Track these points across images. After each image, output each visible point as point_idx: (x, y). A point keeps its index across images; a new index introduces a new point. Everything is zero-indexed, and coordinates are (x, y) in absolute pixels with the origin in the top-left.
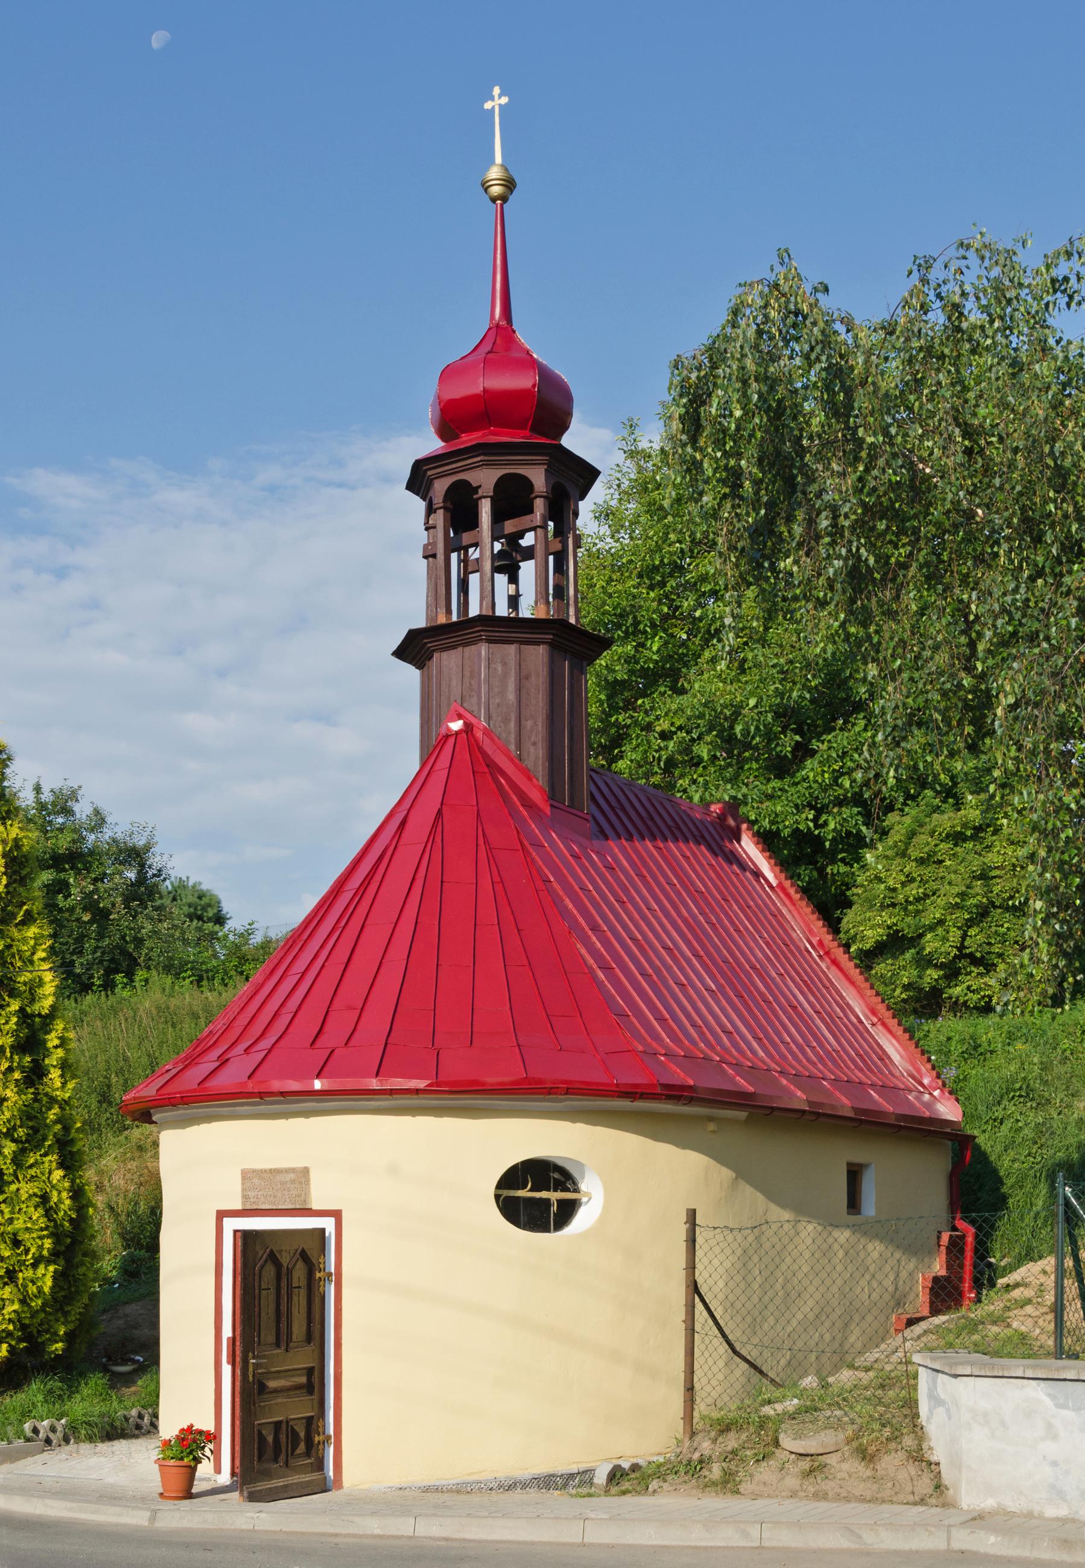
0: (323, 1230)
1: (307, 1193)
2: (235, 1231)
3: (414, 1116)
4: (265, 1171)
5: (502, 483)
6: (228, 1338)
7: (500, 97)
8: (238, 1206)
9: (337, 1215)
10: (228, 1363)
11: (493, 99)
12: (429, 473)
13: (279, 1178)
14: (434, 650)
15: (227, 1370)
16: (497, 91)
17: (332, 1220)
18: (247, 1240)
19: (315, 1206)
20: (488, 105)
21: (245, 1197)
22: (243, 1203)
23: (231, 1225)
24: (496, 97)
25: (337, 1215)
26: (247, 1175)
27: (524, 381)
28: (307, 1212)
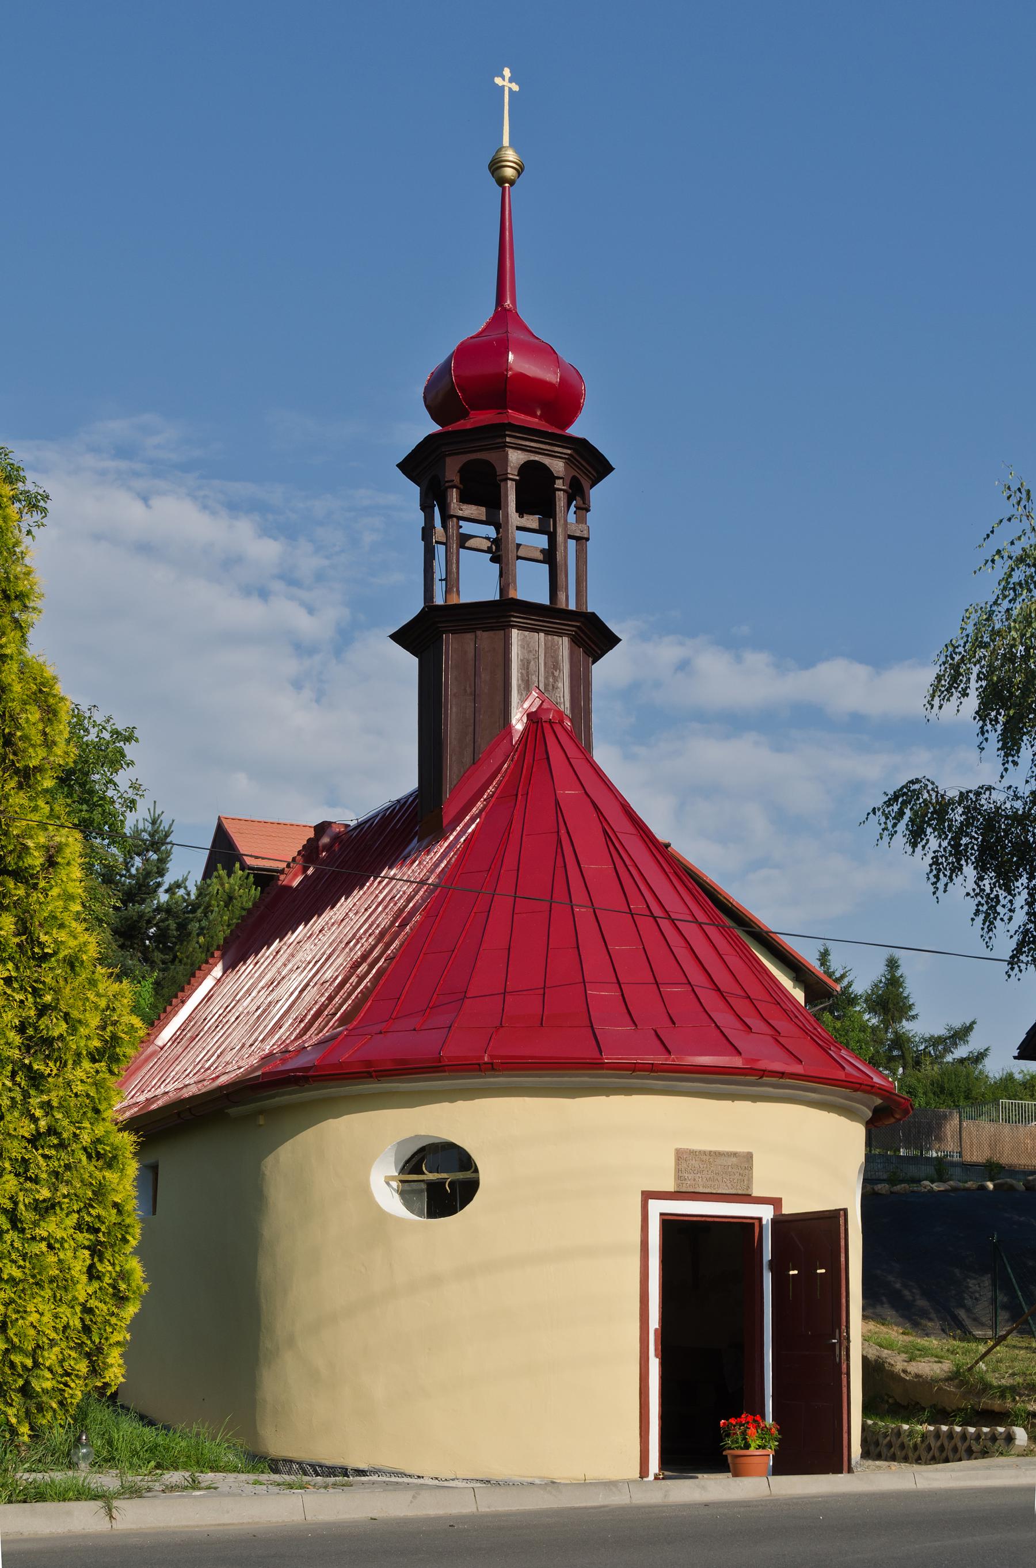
0: (760, 1219)
1: (750, 1179)
3: (608, 1096)
5: (526, 468)
6: (656, 1330)
7: (510, 81)
8: (670, 1186)
10: (656, 1356)
11: (511, 81)
12: (508, 439)
13: (720, 1161)
14: (514, 627)
16: (507, 72)
17: (651, 1202)
18: (671, 1225)
19: (756, 1193)
20: (498, 81)
21: (679, 1177)
23: (657, 1208)
24: (507, 79)
26: (680, 1156)
27: (552, 377)
28: (746, 1198)
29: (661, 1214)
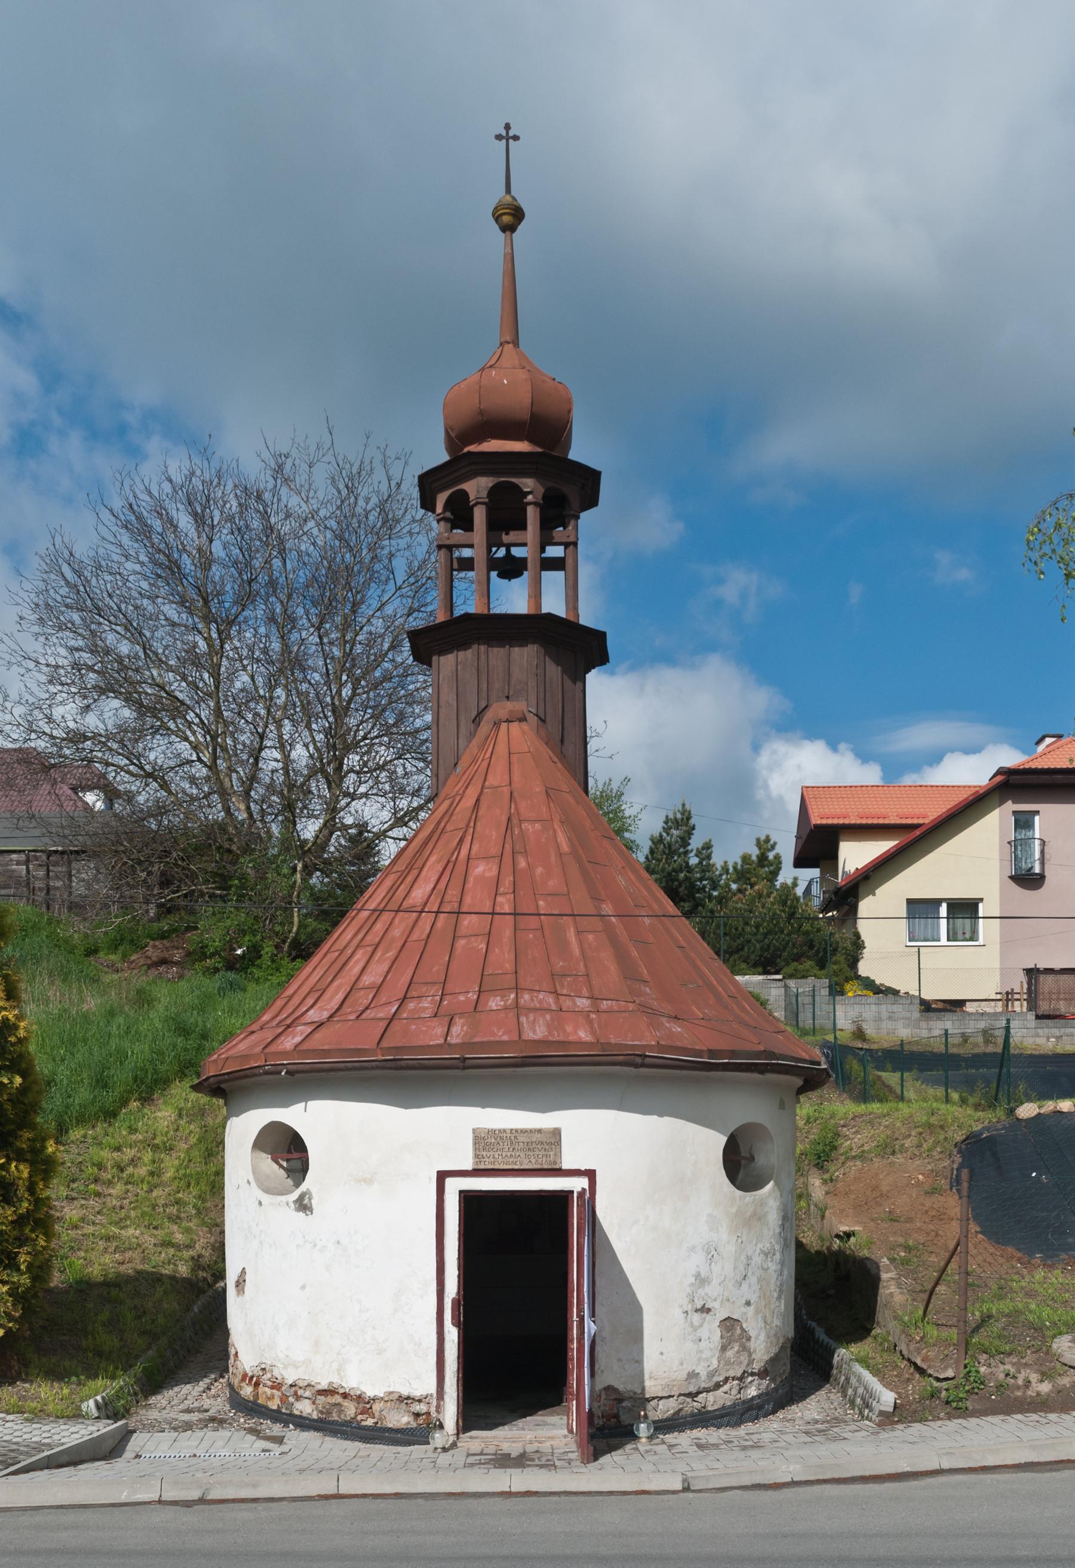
2: (461, 1192)
4: (505, 1131)
6: (453, 1300)
8: (469, 1166)
9: (591, 1174)
15: (452, 1334)
18: (468, 1198)
19: (565, 1166)
25: (591, 1174)
28: (558, 1172)
29: (461, 1192)
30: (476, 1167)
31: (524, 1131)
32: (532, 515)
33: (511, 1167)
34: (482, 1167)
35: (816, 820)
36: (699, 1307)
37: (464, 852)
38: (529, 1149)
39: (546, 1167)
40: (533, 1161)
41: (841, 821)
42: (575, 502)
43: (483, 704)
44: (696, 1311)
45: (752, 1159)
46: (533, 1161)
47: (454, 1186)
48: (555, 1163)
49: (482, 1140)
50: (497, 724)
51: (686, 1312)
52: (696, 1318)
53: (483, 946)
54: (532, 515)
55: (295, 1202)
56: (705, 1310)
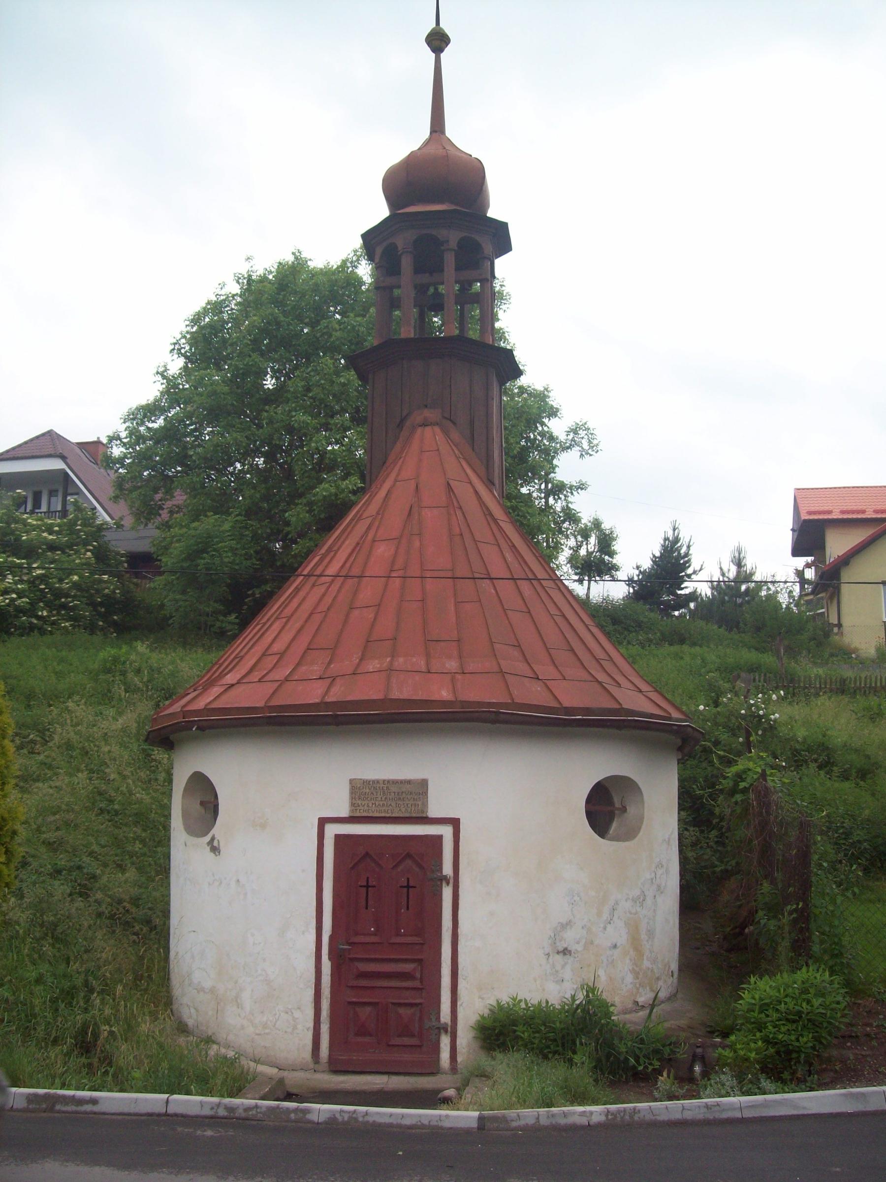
1: (425, 805)
4: (378, 782)
8: (344, 813)
9: (455, 823)
12: (879, 684)
18: (437, 840)
22: (352, 811)
30: (352, 815)
31: (395, 782)
32: (450, 260)
33: (383, 815)
34: (358, 814)
35: (805, 516)
36: (560, 949)
37: (370, 537)
38: (400, 799)
39: (414, 815)
40: (403, 810)
41: (826, 517)
42: (488, 248)
43: (404, 414)
44: (558, 953)
45: (624, 809)
46: (403, 810)
47: (332, 830)
48: (423, 812)
49: (360, 790)
50: (414, 429)
51: (548, 954)
52: (559, 958)
53: (372, 616)
54: (450, 260)
55: (208, 844)
56: (565, 952)
